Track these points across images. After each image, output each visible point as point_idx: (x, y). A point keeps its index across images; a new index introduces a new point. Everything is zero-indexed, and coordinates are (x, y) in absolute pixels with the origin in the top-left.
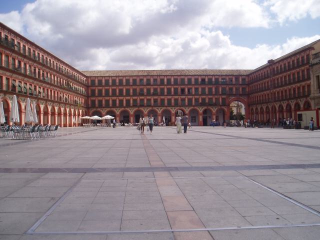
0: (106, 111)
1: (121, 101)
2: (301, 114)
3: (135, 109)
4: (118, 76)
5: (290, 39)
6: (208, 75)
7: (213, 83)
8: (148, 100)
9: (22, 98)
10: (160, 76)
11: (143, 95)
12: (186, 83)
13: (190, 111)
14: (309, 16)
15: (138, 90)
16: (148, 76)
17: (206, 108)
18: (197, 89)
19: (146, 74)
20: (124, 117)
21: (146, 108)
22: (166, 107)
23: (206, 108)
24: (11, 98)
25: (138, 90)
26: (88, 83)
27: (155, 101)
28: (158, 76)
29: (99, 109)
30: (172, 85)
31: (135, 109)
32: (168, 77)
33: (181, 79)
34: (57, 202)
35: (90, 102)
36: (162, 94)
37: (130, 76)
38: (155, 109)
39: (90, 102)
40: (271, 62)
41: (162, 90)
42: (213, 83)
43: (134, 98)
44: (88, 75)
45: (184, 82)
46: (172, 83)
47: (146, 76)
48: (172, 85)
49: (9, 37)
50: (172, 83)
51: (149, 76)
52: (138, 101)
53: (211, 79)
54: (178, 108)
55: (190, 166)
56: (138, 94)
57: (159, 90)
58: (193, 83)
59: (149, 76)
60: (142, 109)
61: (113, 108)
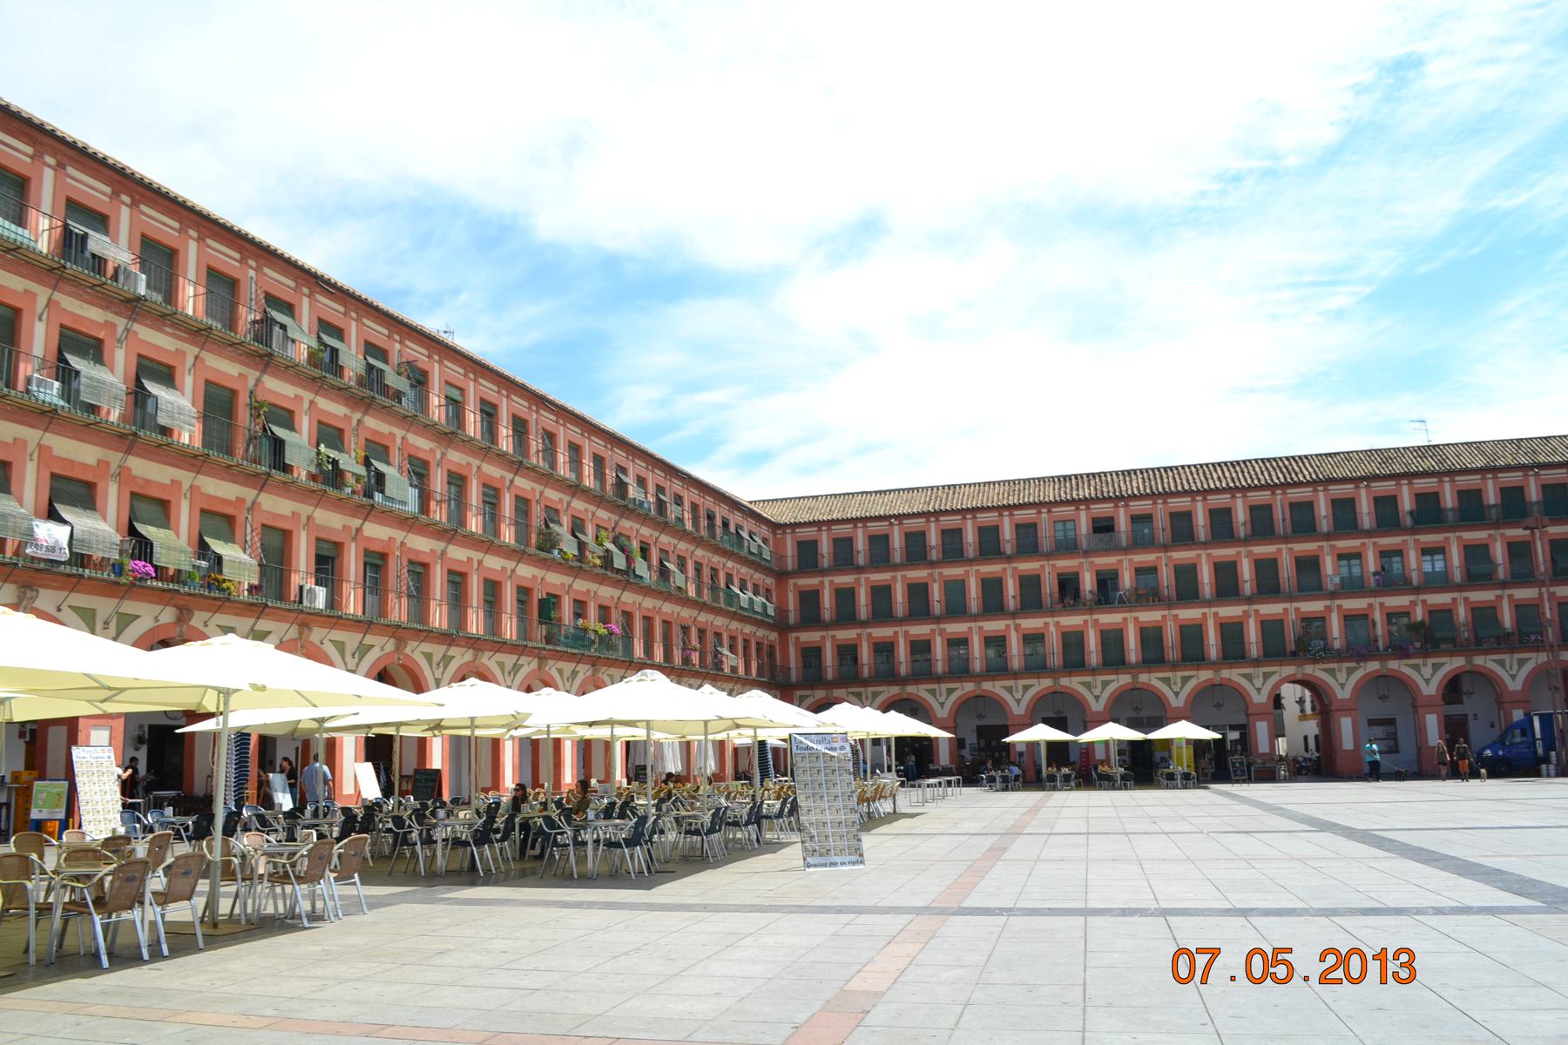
4: (938, 513)
6: (1452, 473)
8: (1349, 618)
9: (561, 664)
10: (1167, 495)
13: (1364, 686)
14: (932, 762)
16: (1096, 500)
17: (1458, 662)
19: (1085, 492)
23: (1458, 662)
24: (508, 667)
26: (781, 558)
28: (1153, 496)
33: (1294, 506)
35: (791, 596)
37: (1000, 509)
39: (791, 596)
40: (649, 888)
44: (784, 520)
47: (1087, 501)
51: (1105, 500)
52: (1054, 642)
53: (1477, 493)
54: (1289, 670)
55: (1335, 919)
59: (1105, 500)
61: (993, 679)
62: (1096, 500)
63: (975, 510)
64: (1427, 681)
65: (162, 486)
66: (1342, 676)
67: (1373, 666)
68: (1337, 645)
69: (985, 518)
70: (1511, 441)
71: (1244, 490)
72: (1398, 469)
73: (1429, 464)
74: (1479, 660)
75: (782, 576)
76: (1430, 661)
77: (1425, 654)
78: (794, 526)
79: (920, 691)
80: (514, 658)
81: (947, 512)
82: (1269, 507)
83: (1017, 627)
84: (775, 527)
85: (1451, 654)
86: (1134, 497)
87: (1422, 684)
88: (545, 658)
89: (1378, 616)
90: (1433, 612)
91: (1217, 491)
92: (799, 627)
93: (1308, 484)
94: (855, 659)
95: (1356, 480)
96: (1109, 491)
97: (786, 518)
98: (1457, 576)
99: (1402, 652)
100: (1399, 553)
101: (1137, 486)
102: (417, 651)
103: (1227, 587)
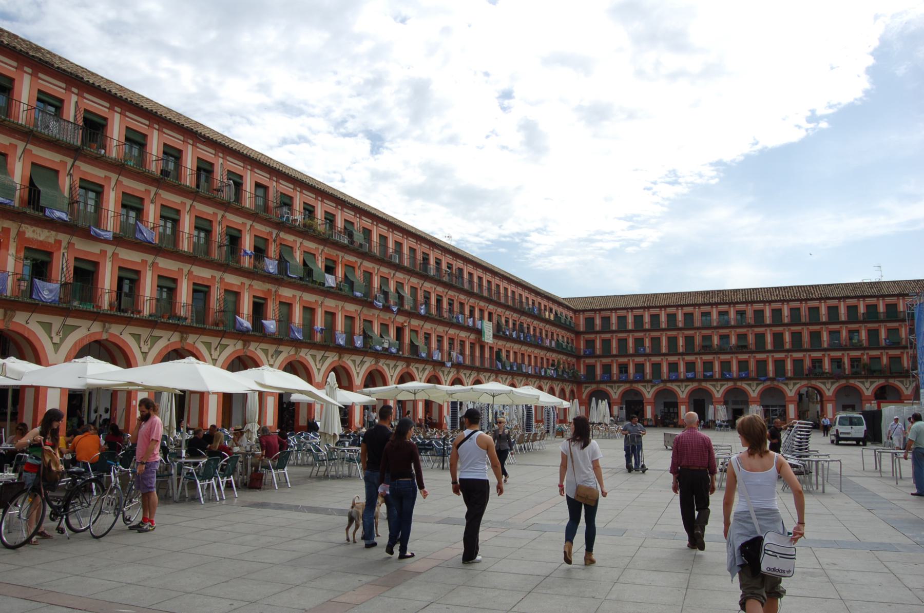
0: (689, 388)
1: (656, 367)
2: (460, 479)
3: (624, 387)
4: (649, 308)
5: (867, 92)
6: (883, 296)
7: (882, 317)
10: (752, 302)
11: (592, 355)
12: (824, 319)
15: (698, 340)
17: (880, 382)
18: (639, 342)
20: (666, 405)
21: (719, 384)
22: (773, 379)
23: (880, 382)
25: (698, 340)
26: (578, 349)
27: (743, 365)
28: (746, 303)
29: (603, 386)
30: (680, 329)
31: (624, 387)
32: (670, 310)
33: (756, 312)
34: (727, 523)
35: (582, 366)
36: (760, 346)
37: (677, 306)
38: (744, 385)
39: (582, 366)
41: (760, 338)
42: (882, 317)
43: (689, 358)
45: (659, 323)
46: (768, 321)
48: (680, 329)
49: (357, 226)
50: (786, 320)
56: (697, 349)
57: (751, 339)
58: (768, 321)
60: (708, 385)
62: (721, 304)
63: (665, 307)
64: (867, 389)
65: (208, 279)
66: (828, 386)
67: (843, 382)
68: (735, 375)
69: (670, 310)
70: (914, 281)
71: (788, 301)
72: (858, 293)
73: (875, 291)
74: (891, 381)
75: (578, 358)
76: (869, 380)
77: (867, 378)
78: (584, 311)
79: (306, 355)
80: (361, 358)
81: (653, 307)
82: (692, 314)
83: (683, 360)
84: (575, 311)
85: (879, 377)
86: (737, 303)
87: (865, 390)
88: (249, 342)
89: (846, 360)
90: (872, 358)
91: (776, 301)
92: (586, 356)
93: (817, 299)
94: (626, 372)
95: (839, 298)
96: (727, 299)
97: (579, 307)
98: (865, 343)
99: (855, 375)
100: (858, 331)
101: (740, 297)
102: (125, 335)
103: (797, 344)
